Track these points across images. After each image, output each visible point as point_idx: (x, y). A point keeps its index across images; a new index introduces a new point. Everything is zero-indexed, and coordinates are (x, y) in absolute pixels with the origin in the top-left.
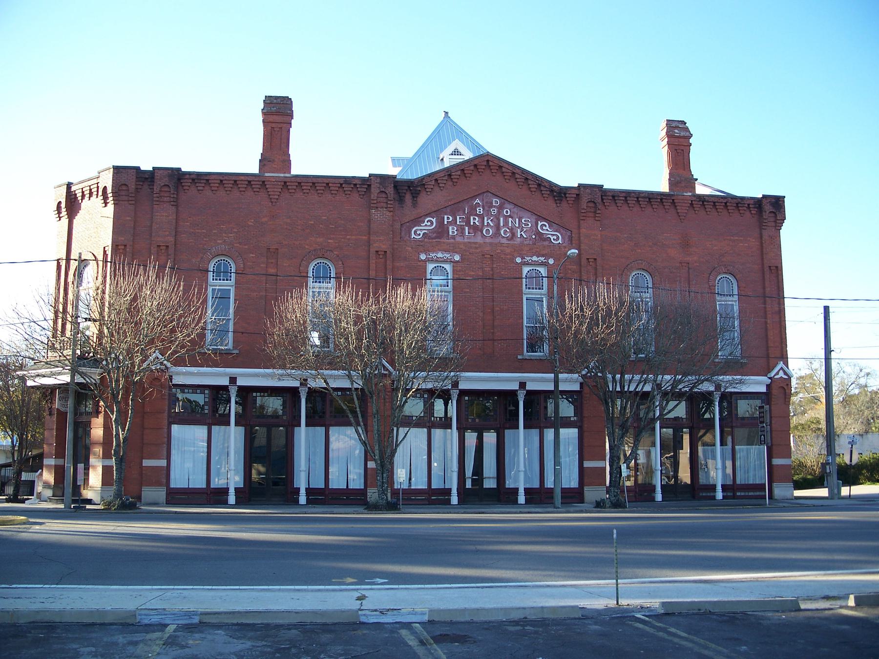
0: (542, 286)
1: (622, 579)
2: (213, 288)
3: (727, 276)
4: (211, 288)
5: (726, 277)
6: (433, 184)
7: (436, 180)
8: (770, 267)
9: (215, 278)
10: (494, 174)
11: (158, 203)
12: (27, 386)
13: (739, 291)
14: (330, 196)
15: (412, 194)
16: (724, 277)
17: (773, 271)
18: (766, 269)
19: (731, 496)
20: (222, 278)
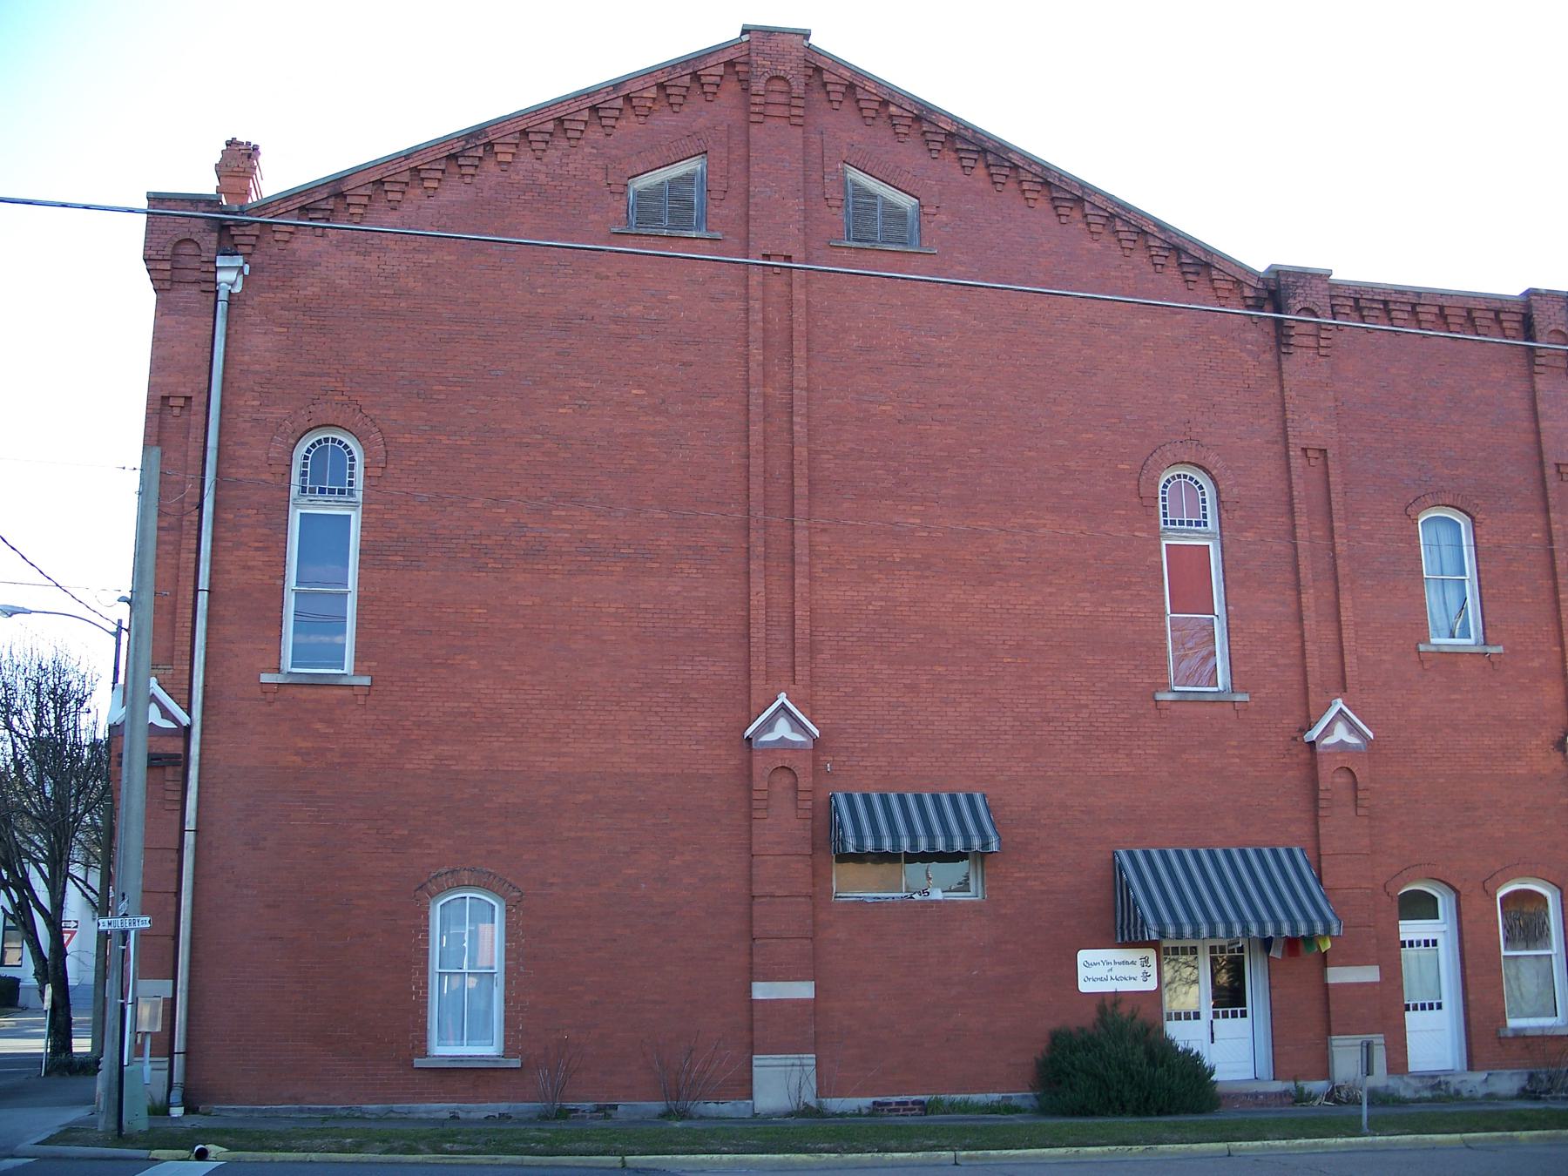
0: (1205, 516)
1: (768, 978)
2: (303, 511)
3: (1189, 474)
4: (299, 511)
5: (1185, 476)
6: (586, 119)
7: (628, 98)
8: (1558, 465)
9: (1169, 519)
10: (836, 105)
11: (760, 118)
12: (423, 890)
13: (1224, 515)
14: (565, 144)
15: (988, 166)
16: (1179, 476)
17: (1313, 462)
18: (1550, 472)
19: (845, 848)
20: (1186, 520)
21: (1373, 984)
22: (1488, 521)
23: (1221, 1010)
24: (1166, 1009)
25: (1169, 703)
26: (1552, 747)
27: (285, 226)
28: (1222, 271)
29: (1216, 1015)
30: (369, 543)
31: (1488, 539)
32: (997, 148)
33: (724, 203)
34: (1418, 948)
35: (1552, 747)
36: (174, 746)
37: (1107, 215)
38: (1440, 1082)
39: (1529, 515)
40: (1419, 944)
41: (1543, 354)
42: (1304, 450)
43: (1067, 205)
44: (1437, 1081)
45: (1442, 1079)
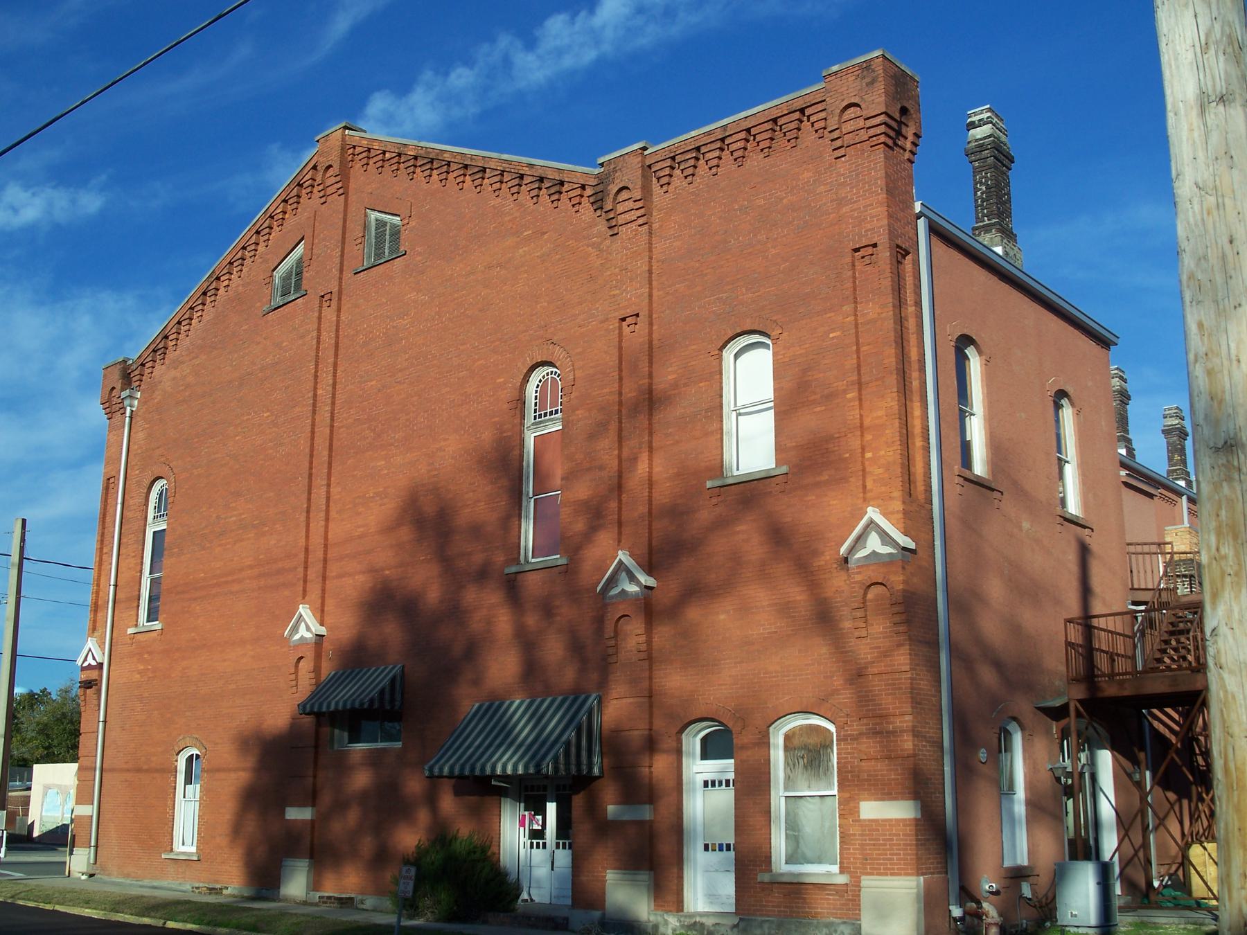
21: (292, 805)
22: (785, 334)
23: (561, 842)
24: (732, 853)
25: (514, 575)
26: (835, 566)
27: (712, 145)
28: (570, 182)
29: (558, 846)
30: (889, 391)
31: (784, 354)
32: (438, 154)
33: (310, 268)
34: (720, 788)
35: (835, 566)
36: (93, 675)
37: (499, 172)
38: (695, 922)
39: (828, 315)
40: (720, 783)
41: (612, 216)
42: (637, 315)
43: (477, 177)
44: (693, 921)
45: (698, 919)
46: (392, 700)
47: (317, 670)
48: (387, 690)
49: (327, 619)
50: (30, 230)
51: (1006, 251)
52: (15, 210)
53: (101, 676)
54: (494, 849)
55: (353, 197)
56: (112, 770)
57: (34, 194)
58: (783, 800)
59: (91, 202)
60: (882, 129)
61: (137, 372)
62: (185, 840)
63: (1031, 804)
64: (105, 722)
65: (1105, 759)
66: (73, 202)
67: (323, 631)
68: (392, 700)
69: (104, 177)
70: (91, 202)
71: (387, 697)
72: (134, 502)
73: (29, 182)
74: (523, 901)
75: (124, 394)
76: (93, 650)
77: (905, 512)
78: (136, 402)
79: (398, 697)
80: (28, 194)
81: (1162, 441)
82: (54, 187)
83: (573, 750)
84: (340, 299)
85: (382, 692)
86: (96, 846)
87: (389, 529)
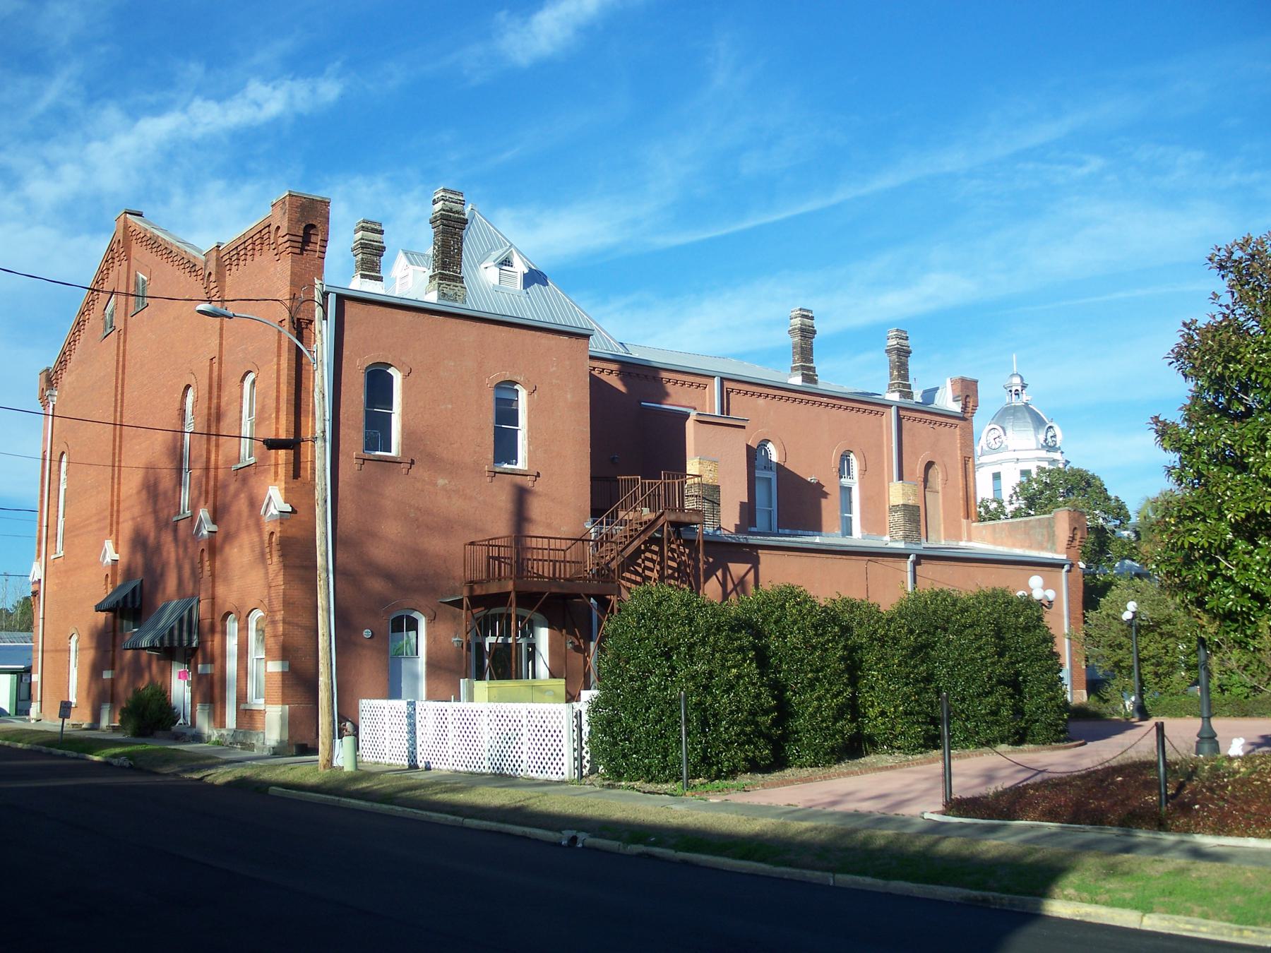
46: (134, 602)
47: (113, 582)
48: (130, 596)
49: (120, 550)
50: (275, 124)
51: (300, 337)
52: (259, 105)
53: (40, 588)
54: (168, 693)
55: (133, 261)
56: (47, 651)
57: (274, 88)
58: (255, 660)
59: (330, 90)
60: (288, 244)
61: (54, 378)
62: (565, 769)
63: (432, 665)
64: (44, 618)
65: (543, 636)
66: (313, 91)
67: (117, 557)
68: (134, 602)
69: (338, 64)
70: (330, 90)
71: (129, 599)
72: (55, 468)
73: (269, 78)
74: (181, 724)
75: (48, 393)
76: (37, 572)
77: (286, 488)
78: (55, 398)
79: (138, 600)
80: (269, 89)
81: (885, 359)
82: (293, 79)
83: (176, 632)
84: (125, 334)
85: (126, 597)
86: (41, 701)
87: (139, 492)
